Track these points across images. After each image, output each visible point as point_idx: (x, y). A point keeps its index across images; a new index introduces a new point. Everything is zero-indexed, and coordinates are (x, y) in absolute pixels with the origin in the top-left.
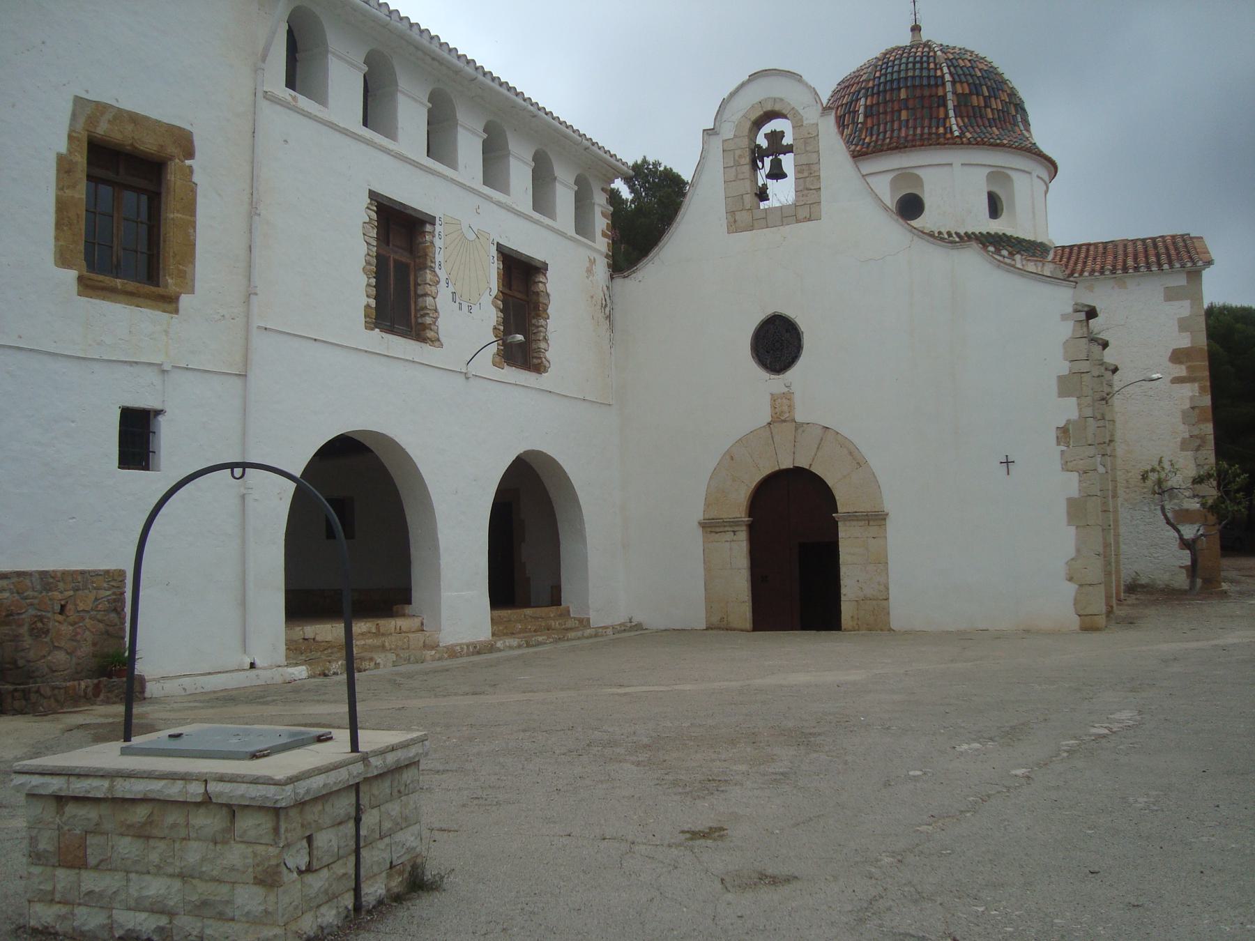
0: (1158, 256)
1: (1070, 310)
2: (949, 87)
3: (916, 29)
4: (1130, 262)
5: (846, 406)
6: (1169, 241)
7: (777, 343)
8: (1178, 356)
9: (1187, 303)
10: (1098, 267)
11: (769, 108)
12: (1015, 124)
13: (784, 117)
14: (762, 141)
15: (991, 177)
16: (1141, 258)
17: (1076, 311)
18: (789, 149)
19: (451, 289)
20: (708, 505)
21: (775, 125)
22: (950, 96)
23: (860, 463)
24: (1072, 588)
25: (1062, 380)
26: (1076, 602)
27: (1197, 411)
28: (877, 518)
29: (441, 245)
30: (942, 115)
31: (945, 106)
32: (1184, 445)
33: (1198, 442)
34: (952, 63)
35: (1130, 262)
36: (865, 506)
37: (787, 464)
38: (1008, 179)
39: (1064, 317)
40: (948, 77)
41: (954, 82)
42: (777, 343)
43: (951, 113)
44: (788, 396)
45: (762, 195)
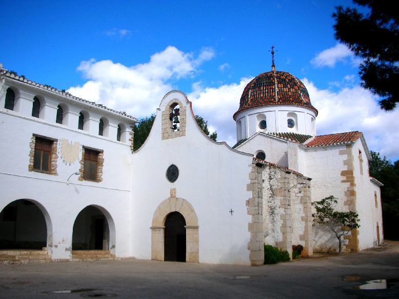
5: (190, 194)
7: (173, 173)
9: (346, 155)
15: (289, 114)
19: (63, 159)
20: (153, 222)
23: (193, 211)
24: (249, 252)
25: (248, 186)
28: (196, 228)
29: (59, 148)
32: (345, 204)
33: (350, 202)
36: (194, 225)
37: (173, 210)
38: (296, 115)
39: (249, 166)
40: (276, 82)
41: (278, 84)
42: (173, 173)
43: (276, 94)
44: (174, 189)
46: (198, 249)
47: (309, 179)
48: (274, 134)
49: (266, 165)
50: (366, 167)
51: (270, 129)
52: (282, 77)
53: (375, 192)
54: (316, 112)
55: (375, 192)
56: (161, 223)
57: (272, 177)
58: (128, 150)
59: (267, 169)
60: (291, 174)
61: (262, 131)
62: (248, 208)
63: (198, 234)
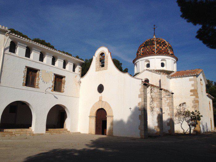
7: (101, 89)
20: (90, 113)
22: (156, 47)
23: (110, 108)
28: (90, 117)
29: (40, 74)
32: (193, 107)
37: (101, 108)
40: (155, 44)
42: (101, 89)
44: (101, 97)
47: (173, 93)
48: (154, 70)
49: (149, 86)
50: (204, 88)
51: (151, 68)
52: (159, 41)
53: (210, 102)
55: (210, 102)
57: (152, 91)
58: (79, 77)
59: (149, 88)
60: (163, 90)
61: (147, 68)
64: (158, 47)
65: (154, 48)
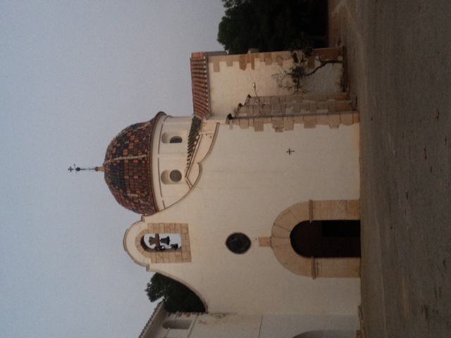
0: (200, 73)
1: (228, 126)
2: (124, 158)
3: (97, 169)
4: (203, 85)
6: (193, 67)
7: (238, 243)
8: (243, 67)
10: (205, 99)
11: (140, 243)
12: (141, 130)
13: (143, 238)
14: (153, 246)
15: (164, 141)
16: (201, 80)
17: (229, 123)
18: (157, 236)
20: (306, 275)
21: (148, 244)
22: (128, 158)
23: (289, 211)
24: (341, 126)
25: (256, 130)
26: (347, 124)
27: (267, 59)
28: (312, 204)
30: (137, 161)
31: (133, 160)
33: (279, 59)
34: (114, 156)
35: (203, 85)
37: (288, 241)
39: (231, 128)
40: (120, 158)
41: (123, 156)
42: (238, 243)
43: (136, 157)
44: (260, 240)
45: (175, 247)
46: (342, 201)
47: (249, 96)
54: (160, 114)
56: (306, 262)
58: (203, 317)
62: (286, 130)
63: (320, 202)
64: (131, 152)
65: (131, 161)
